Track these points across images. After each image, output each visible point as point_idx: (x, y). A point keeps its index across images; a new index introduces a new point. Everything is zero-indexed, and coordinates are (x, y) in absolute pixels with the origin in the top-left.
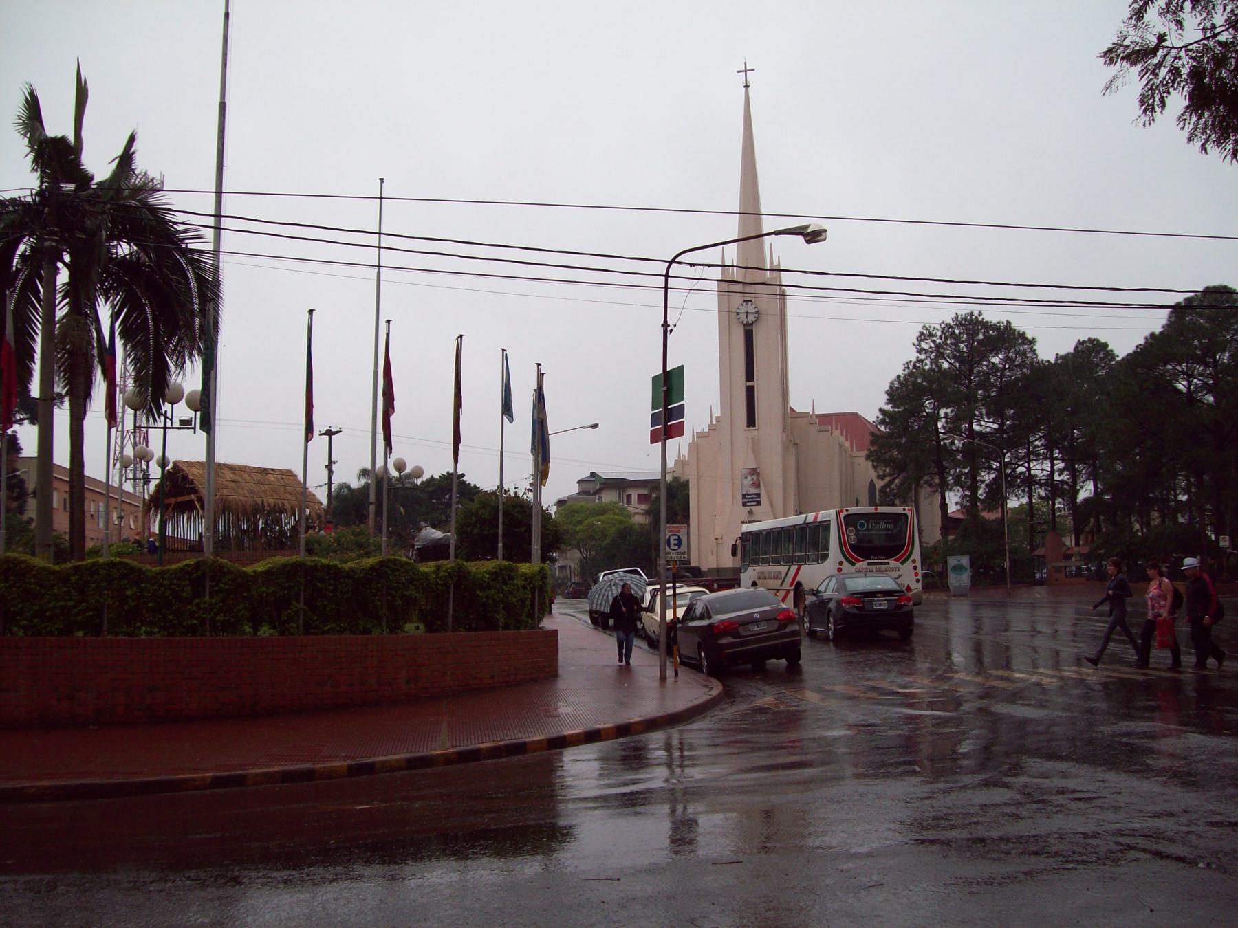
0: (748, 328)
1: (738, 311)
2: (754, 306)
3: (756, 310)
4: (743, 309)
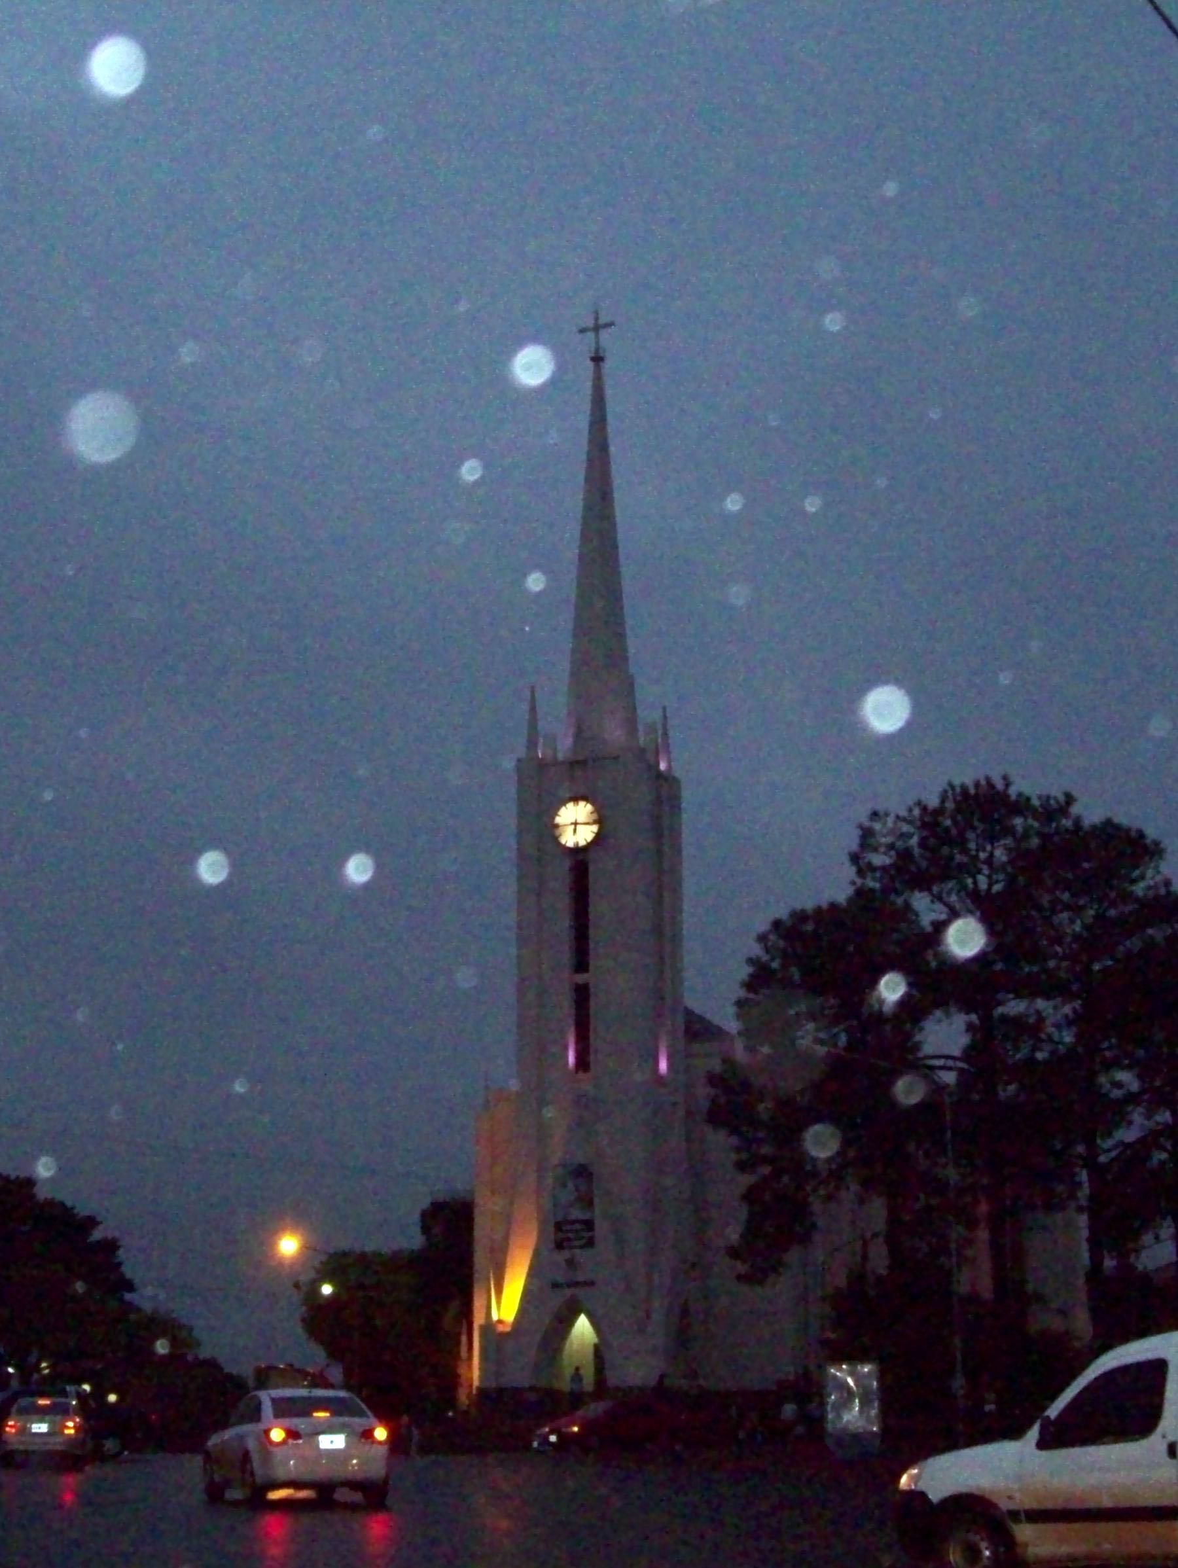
0: (580, 857)
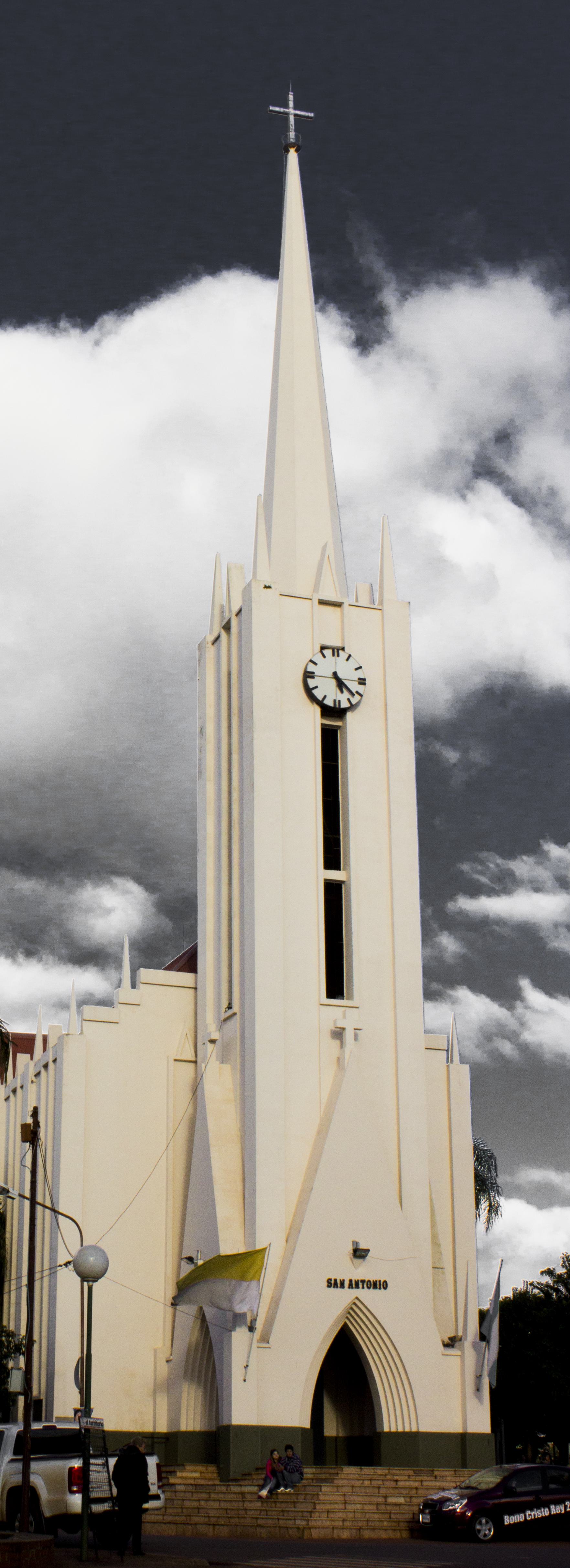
1: (311, 668)
2: (353, 664)
3: (360, 674)
4: (325, 666)
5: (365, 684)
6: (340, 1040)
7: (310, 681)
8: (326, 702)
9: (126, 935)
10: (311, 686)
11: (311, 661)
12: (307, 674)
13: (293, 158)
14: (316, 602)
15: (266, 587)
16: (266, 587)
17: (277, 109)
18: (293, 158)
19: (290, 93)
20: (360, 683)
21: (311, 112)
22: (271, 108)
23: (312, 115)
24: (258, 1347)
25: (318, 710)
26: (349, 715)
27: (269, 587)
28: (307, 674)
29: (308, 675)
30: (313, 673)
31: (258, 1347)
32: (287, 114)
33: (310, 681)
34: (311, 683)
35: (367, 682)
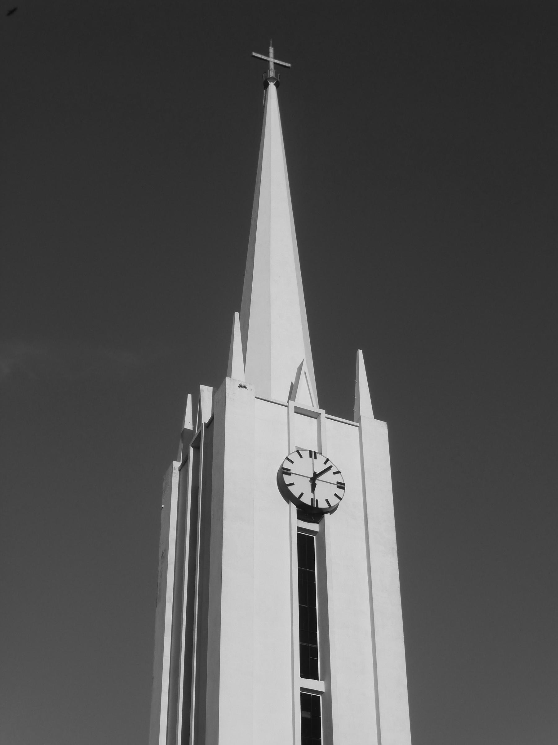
1: (287, 465)
5: (344, 488)
6: (239, 313)
7: (285, 477)
8: (303, 499)
9: (322, 689)
10: (287, 482)
11: (287, 458)
12: (284, 470)
13: (272, 89)
14: (292, 410)
15: (240, 386)
16: (240, 386)
17: (259, 56)
18: (272, 89)
19: (271, 48)
20: (338, 487)
21: (288, 62)
22: (254, 54)
23: (289, 65)
24: (326, 418)
25: (294, 508)
26: (327, 516)
27: (245, 387)
28: (284, 470)
29: (284, 471)
30: (289, 470)
31: (326, 418)
32: (268, 62)
33: (285, 477)
34: (287, 479)
35: (346, 487)
